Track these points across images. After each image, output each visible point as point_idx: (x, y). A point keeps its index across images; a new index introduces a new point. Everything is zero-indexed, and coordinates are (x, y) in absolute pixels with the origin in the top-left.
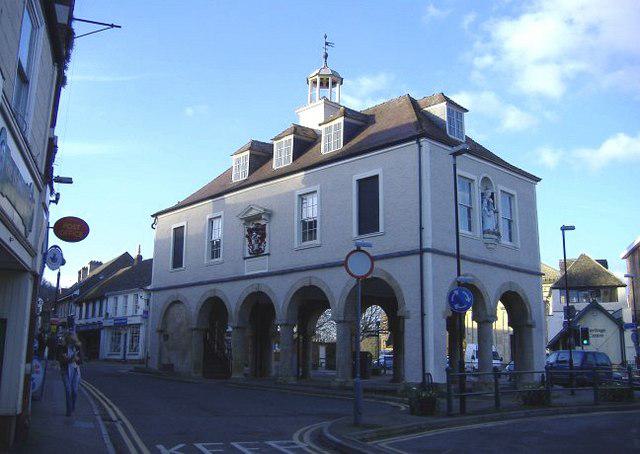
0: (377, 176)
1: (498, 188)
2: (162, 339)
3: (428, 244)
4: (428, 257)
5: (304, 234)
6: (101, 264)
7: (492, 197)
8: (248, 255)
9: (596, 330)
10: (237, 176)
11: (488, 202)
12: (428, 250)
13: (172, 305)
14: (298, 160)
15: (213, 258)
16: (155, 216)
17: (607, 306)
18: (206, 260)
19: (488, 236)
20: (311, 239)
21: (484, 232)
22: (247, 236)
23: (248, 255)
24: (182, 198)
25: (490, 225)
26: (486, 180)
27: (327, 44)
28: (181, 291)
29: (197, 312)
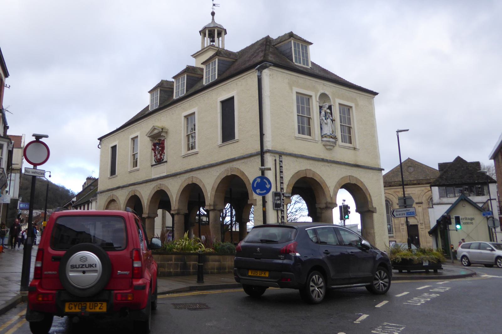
1: (336, 103)
7: (330, 108)
8: (154, 163)
9: (466, 219)
10: (178, 93)
11: (326, 113)
12: (269, 151)
15: (134, 167)
16: (100, 139)
17: (476, 199)
19: (325, 139)
21: (322, 137)
22: (153, 149)
23: (154, 163)
25: (327, 130)
26: (324, 96)
27: (214, 5)
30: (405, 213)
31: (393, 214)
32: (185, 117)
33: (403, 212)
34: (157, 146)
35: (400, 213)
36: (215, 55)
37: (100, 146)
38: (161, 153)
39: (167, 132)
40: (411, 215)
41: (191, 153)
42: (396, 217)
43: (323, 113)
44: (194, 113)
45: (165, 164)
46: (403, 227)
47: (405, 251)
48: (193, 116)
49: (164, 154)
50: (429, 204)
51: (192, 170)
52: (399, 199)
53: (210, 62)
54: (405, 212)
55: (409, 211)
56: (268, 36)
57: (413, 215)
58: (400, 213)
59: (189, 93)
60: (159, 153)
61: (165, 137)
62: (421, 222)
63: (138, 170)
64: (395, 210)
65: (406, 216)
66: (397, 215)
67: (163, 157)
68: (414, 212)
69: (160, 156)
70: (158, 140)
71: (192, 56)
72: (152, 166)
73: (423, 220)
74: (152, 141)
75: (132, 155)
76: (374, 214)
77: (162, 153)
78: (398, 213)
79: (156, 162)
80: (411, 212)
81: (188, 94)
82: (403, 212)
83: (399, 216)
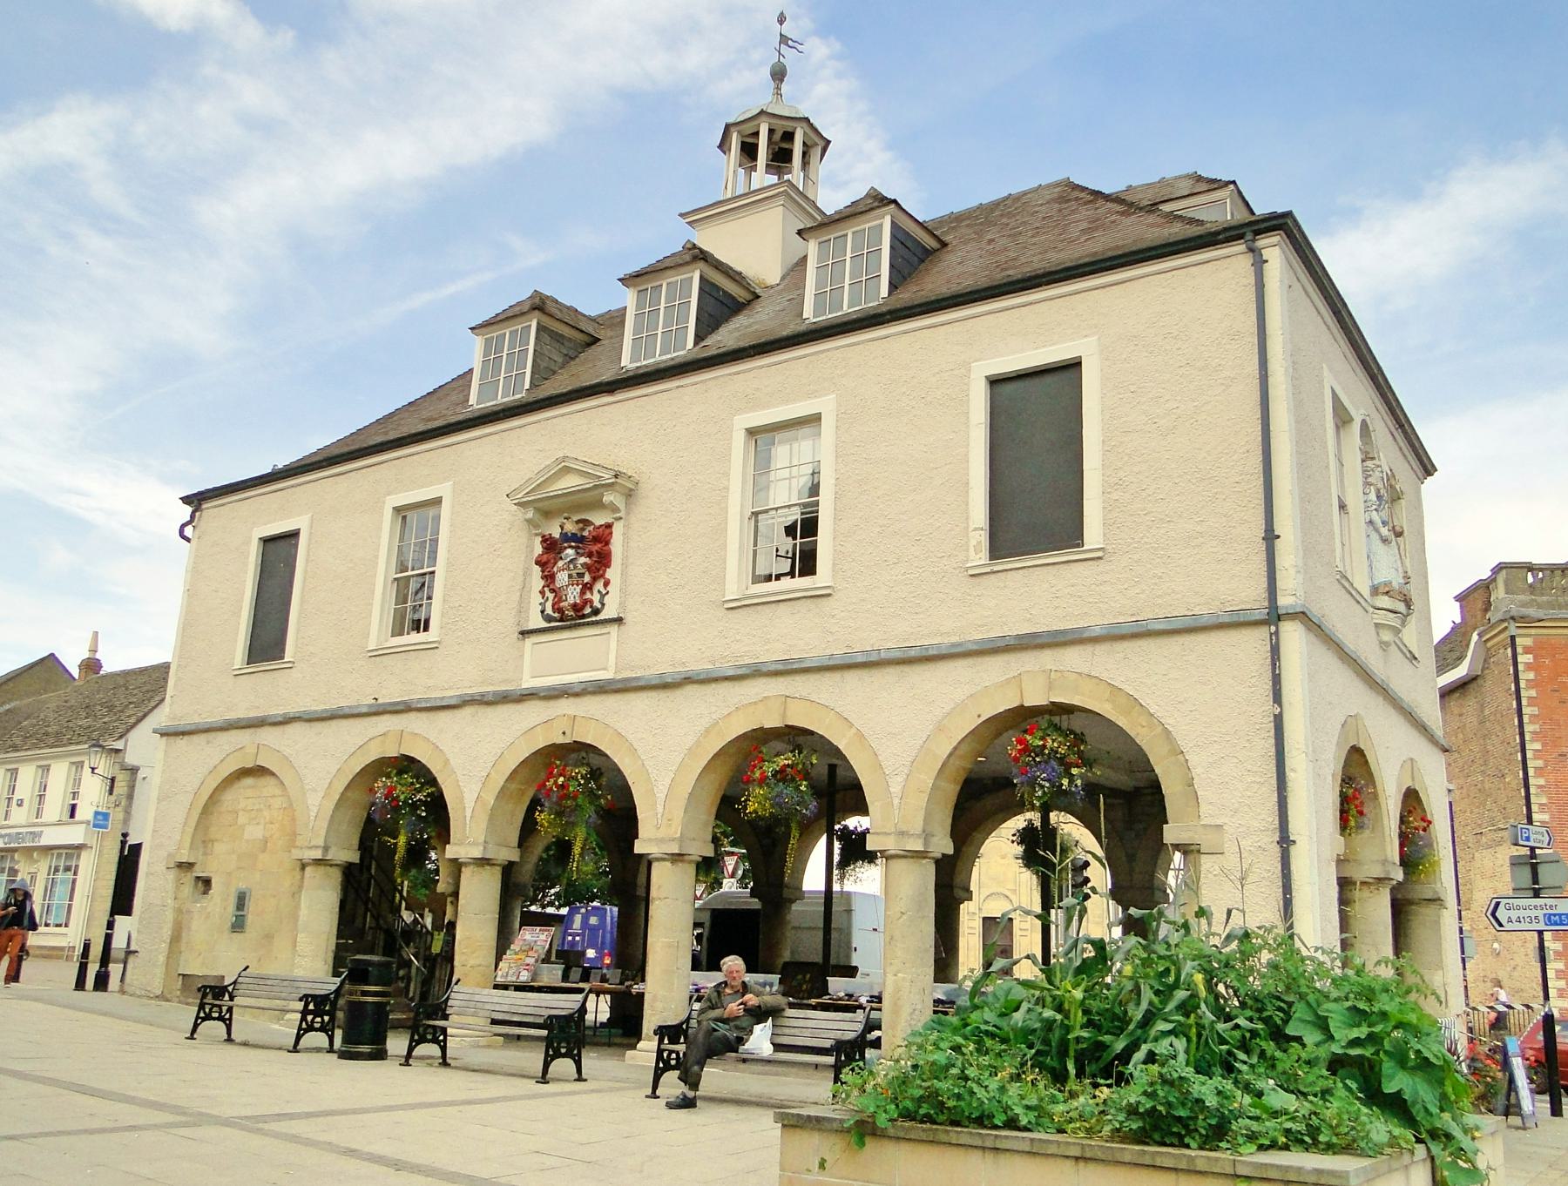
3: (1284, 601)
4: (1293, 636)
5: (399, 618)
6: (795, 523)
8: (537, 622)
13: (245, 773)
14: (709, 341)
16: (196, 501)
19: (1384, 601)
23: (537, 622)
27: (784, 39)
28: (268, 736)
30: (1541, 918)
31: (1493, 914)
32: (397, 510)
33: (1533, 913)
34: (570, 547)
35: (1522, 913)
36: (526, 307)
37: (188, 531)
38: (587, 578)
39: (631, 490)
41: (777, 594)
42: (1508, 926)
43: (1373, 496)
44: (437, 502)
45: (613, 629)
48: (431, 512)
49: (606, 584)
51: (404, 708)
52: (1512, 864)
54: (1540, 913)
58: (1522, 913)
60: (576, 578)
61: (617, 510)
63: (433, 648)
64: (1503, 901)
65: (1541, 927)
66: (1510, 920)
69: (583, 593)
70: (578, 522)
71: (681, 215)
72: (525, 633)
74: (537, 526)
75: (391, 579)
77: (595, 579)
78: (1514, 914)
79: (548, 619)
80: (1560, 915)
81: (531, 400)
82: (1533, 913)
83: (1517, 926)
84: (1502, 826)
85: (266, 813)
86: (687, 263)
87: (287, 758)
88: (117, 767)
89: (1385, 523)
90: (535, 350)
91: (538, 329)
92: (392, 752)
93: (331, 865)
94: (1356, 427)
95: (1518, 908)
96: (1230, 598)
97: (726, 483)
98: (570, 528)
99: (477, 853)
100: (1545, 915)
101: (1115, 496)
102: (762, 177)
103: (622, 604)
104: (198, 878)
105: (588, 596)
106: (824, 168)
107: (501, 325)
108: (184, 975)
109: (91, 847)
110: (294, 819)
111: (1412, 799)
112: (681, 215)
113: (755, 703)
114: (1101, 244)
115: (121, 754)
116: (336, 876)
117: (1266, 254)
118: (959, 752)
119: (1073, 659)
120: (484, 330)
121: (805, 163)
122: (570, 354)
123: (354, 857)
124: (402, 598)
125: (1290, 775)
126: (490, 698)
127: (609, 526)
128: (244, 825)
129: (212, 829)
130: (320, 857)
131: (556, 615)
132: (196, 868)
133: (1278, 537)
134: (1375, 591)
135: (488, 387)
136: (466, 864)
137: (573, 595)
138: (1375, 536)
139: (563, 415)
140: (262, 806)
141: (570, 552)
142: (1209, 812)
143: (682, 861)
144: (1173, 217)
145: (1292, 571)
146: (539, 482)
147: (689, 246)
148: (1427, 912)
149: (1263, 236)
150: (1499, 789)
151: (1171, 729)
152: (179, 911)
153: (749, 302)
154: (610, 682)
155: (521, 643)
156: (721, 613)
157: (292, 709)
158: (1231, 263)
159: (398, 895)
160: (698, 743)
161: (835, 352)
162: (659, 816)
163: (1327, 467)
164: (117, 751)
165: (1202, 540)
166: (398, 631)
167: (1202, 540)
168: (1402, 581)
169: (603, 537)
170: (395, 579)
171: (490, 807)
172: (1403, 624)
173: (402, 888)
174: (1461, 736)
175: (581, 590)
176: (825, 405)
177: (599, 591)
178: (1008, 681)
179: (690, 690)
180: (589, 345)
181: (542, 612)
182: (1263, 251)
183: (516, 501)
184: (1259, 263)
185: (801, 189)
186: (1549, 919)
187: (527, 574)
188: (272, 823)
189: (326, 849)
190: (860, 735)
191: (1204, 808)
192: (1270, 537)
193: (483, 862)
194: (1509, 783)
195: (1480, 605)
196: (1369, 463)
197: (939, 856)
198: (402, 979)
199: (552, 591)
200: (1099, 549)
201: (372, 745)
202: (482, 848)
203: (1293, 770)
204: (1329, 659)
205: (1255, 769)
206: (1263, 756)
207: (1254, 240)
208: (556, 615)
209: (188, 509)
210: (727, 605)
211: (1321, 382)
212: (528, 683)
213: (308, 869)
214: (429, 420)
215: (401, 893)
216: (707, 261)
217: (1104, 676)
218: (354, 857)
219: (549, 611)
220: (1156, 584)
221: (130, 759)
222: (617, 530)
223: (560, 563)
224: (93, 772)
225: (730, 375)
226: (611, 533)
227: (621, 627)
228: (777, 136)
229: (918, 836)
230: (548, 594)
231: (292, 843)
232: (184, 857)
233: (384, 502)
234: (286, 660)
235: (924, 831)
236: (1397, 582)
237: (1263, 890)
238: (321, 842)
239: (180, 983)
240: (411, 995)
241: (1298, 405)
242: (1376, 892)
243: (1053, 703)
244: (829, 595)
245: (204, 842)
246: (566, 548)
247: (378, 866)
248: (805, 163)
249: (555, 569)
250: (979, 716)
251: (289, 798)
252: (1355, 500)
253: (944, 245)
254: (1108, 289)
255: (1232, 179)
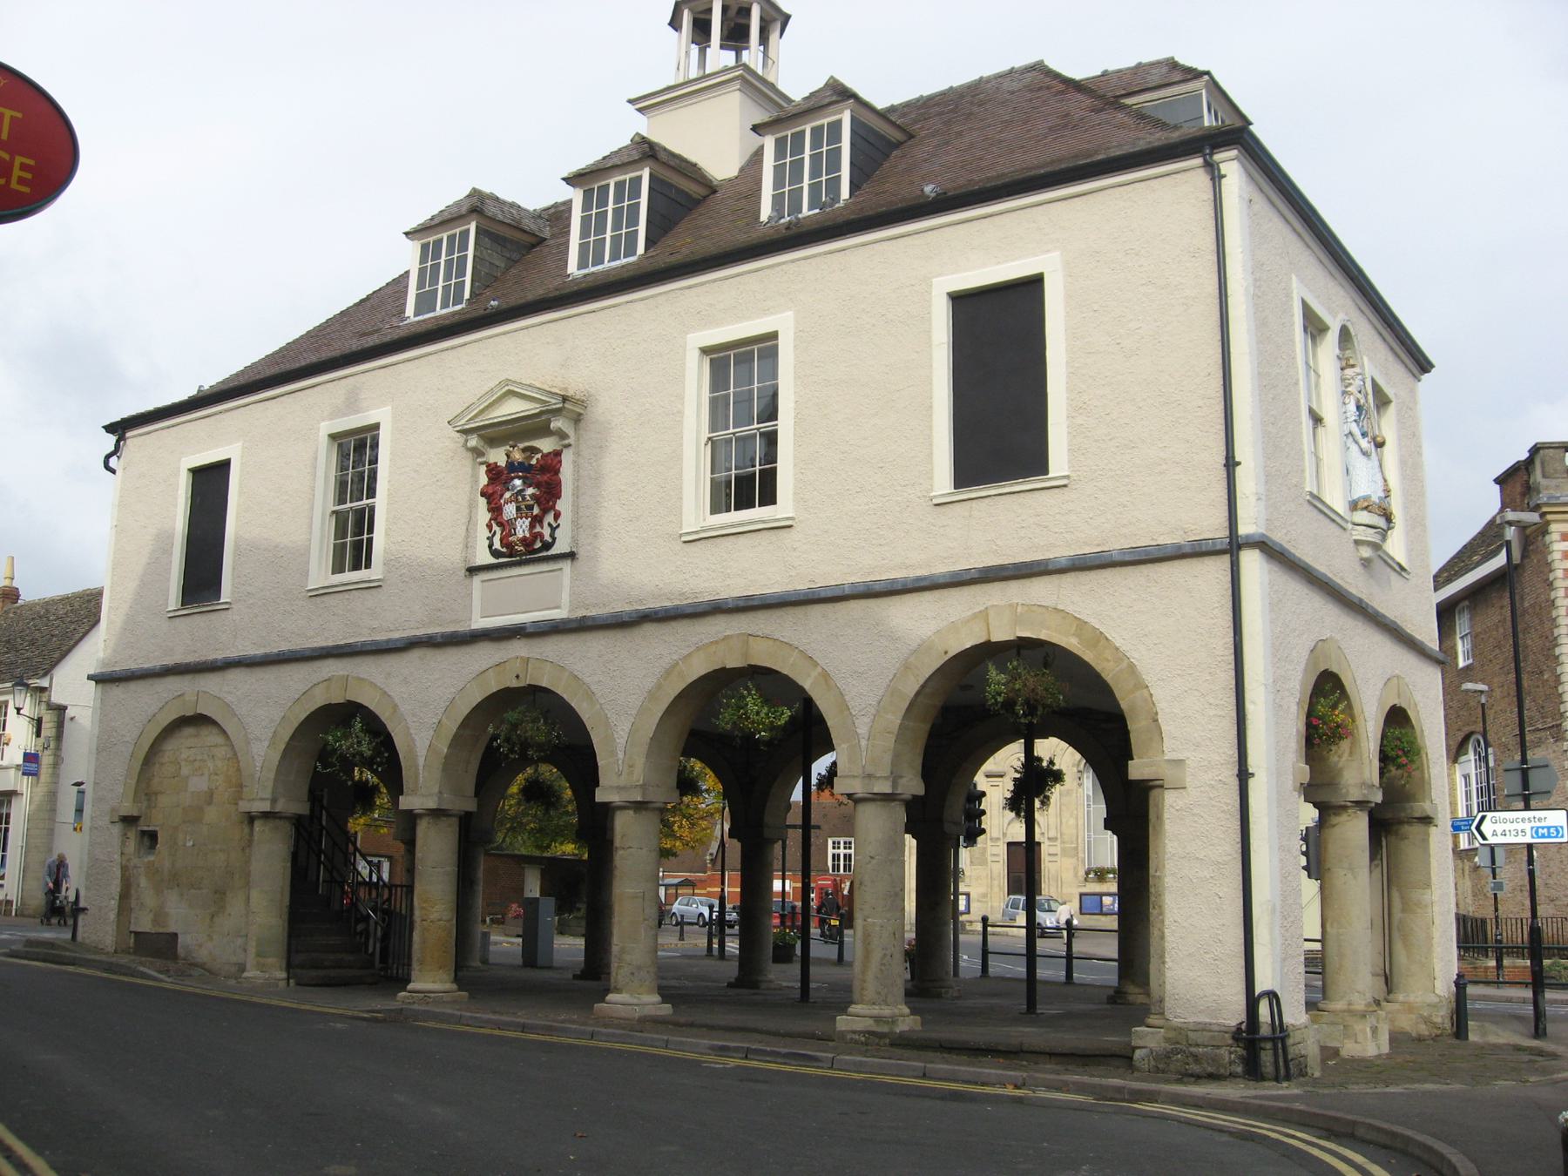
0: (1034, 284)
2: (131, 846)
3: (1245, 529)
4: (1252, 562)
5: (339, 551)
8: (485, 558)
14: (669, 241)
16: (120, 429)
18: (320, 574)
20: (356, 566)
23: (485, 558)
24: (210, 379)
28: (211, 684)
29: (276, 756)
31: (1478, 828)
33: (1520, 826)
34: (519, 478)
35: (1508, 827)
36: (464, 210)
37: (113, 462)
39: (580, 414)
40: (1549, 837)
43: (1352, 407)
46: (995, 850)
47: (127, 850)
49: (557, 516)
50: (1080, 779)
53: (805, 124)
54: (1527, 827)
55: (1543, 824)
56: (1042, 61)
57: (1556, 837)
58: (1508, 827)
59: (664, 258)
62: (1052, 834)
67: (546, 532)
68: (1562, 827)
69: (532, 526)
70: (524, 450)
71: (630, 101)
72: (473, 571)
73: (1056, 828)
76: (1433, 830)
77: (545, 511)
78: (1499, 828)
79: (495, 554)
80: (1549, 828)
81: (475, 314)
82: (1520, 826)
84: (1540, 726)
85: (210, 764)
86: (635, 162)
87: (228, 706)
88: (43, 706)
89: (1364, 435)
90: (474, 256)
91: (477, 233)
92: (338, 699)
93: (280, 818)
94: (1332, 337)
95: (1505, 821)
96: (1193, 527)
97: (680, 406)
98: (518, 456)
99: (432, 804)
100: (1532, 828)
101: (1079, 421)
102: (719, 58)
103: (575, 540)
104: (143, 833)
105: (538, 529)
106: (785, 46)
107: (439, 229)
108: (136, 933)
109: (22, 794)
110: (239, 770)
111: (1397, 718)
112: (630, 101)
113: (716, 642)
114: (1062, 150)
115: (47, 694)
116: (287, 828)
117: (1224, 168)
118: (927, 690)
119: (1039, 591)
120: (417, 235)
121: (764, 40)
122: (513, 257)
123: (303, 808)
124: (340, 531)
125: (1249, 707)
126: (439, 640)
127: (558, 454)
128: (187, 777)
129: (156, 780)
130: (269, 810)
131: (504, 550)
132: (142, 821)
133: (1239, 464)
134: (1354, 506)
135: (425, 302)
136: (420, 816)
137: (522, 528)
138: (1354, 448)
139: (504, 334)
140: (206, 757)
141: (518, 482)
142: (1172, 748)
143: (646, 809)
144: (1141, 116)
145: (1253, 499)
146: (482, 407)
147: (637, 139)
148: (1414, 830)
149: (1222, 149)
150: (1538, 687)
151: (1136, 663)
152: (124, 868)
153: (705, 198)
154: (564, 621)
155: (467, 581)
156: (678, 546)
157: (232, 653)
158: (1187, 177)
159: (350, 846)
160: (659, 687)
161: (791, 265)
162: (620, 762)
163: (1297, 383)
164: (43, 690)
165: (1164, 467)
166: (338, 568)
167: (1164, 467)
168: (1382, 495)
169: (551, 465)
170: (334, 512)
171: (443, 756)
172: (1384, 538)
173: (356, 839)
174: (1501, 630)
175: (530, 523)
176: (782, 322)
177: (550, 525)
178: (975, 616)
179: (649, 629)
180: (533, 246)
181: (490, 546)
182: (1221, 165)
183: (458, 429)
184: (1216, 177)
185: (760, 72)
186: (1537, 832)
187: (472, 506)
188: (216, 774)
189: (274, 801)
190: (825, 675)
191: (1168, 744)
192: (1231, 464)
193: (437, 814)
194: (1547, 681)
195: (1519, 489)
196: (1349, 372)
197: (909, 797)
198: (361, 933)
199: (500, 524)
200: (1064, 477)
201: (317, 691)
202: (436, 799)
203: (1253, 702)
204: (1296, 589)
205: (1218, 702)
206: (1224, 689)
207: (1211, 154)
208: (504, 550)
209: (111, 439)
210: (684, 539)
211: (1289, 296)
212: (480, 623)
213: (258, 825)
214: (364, 334)
215: (354, 844)
216: (657, 159)
217: (1070, 609)
218: (303, 808)
219: (497, 545)
220: (1121, 513)
221: (57, 697)
222: (567, 459)
223: (507, 495)
224: (18, 713)
225: (680, 289)
226: (560, 462)
227: (575, 563)
228: (732, 13)
229: (886, 778)
230: (495, 527)
231: (238, 796)
232: (128, 808)
233: (319, 429)
234: (222, 601)
235: (892, 773)
236: (1376, 494)
237: (1223, 823)
238: (268, 794)
239: (132, 940)
240: (371, 950)
241: (1260, 323)
242: (1353, 815)
243: (1020, 638)
244: (790, 526)
245: (146, 794)
246: (513, 478)
247: (329, 815)
248: (764, 40)
249: (502, 501)
250: (946, 653)
251: (232, 746)
252: (1329, 412)
253: (911, 136)
254: (1070, 200)
255: (1206, 69)
